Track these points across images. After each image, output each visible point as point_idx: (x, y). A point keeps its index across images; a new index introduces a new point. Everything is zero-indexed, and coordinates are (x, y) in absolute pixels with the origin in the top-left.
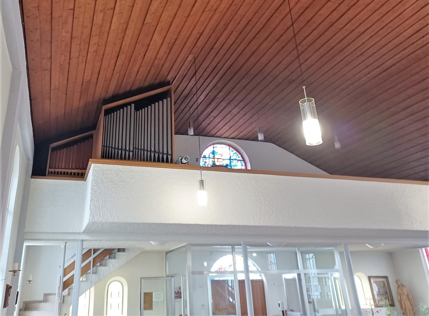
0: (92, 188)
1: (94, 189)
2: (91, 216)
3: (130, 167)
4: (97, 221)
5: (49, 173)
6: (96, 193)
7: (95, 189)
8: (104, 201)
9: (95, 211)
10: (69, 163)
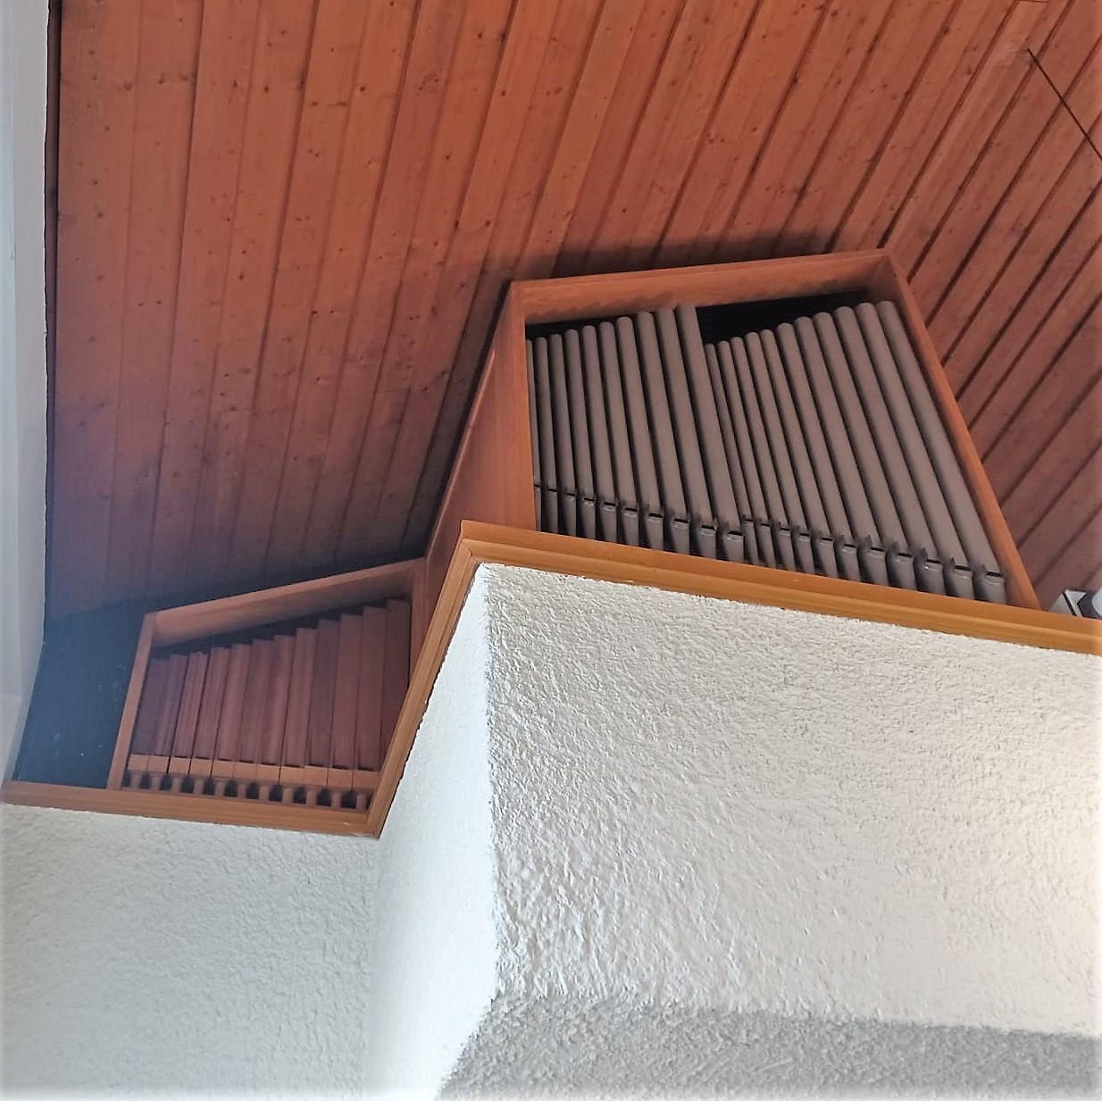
0: (498, 720)
1: (514, 732)
2: (515, 942)
3: (752, 608)
4: (571, 986)
5: (126, 781)
6: (537, 760)
7: (521, 729)
8: (605, 829)
9: (539, 898)
10: (267, 729)
